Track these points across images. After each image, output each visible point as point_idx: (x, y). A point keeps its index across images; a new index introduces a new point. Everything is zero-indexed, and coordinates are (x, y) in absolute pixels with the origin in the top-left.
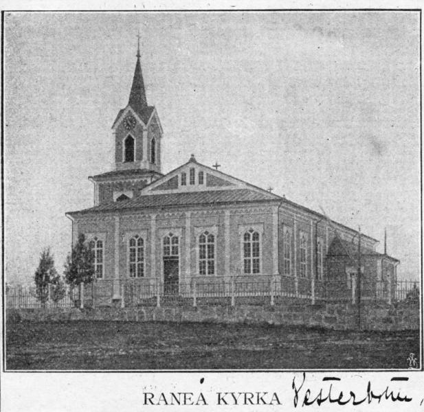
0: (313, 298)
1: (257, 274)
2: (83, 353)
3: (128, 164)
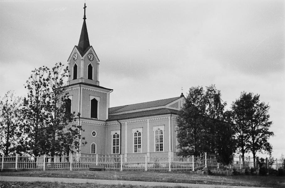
1: (161, 151)
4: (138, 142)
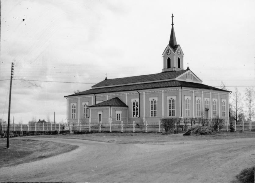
0: (146, 130)
3: (169, 69)
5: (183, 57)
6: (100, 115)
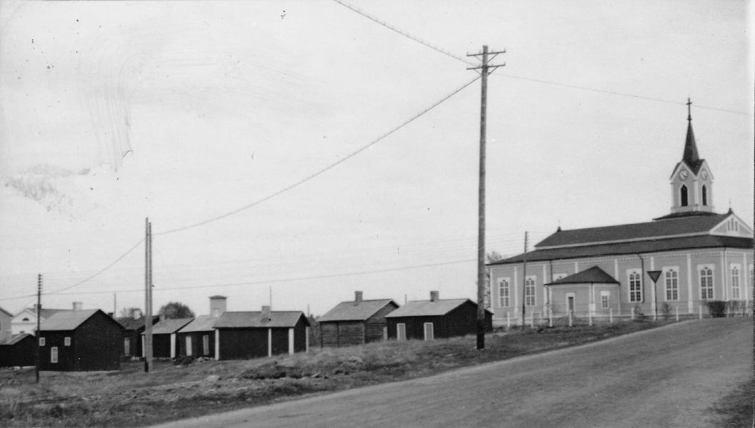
1: (675, 300)
2: (158, 397)
3: (686, 207)
4: (504, 292)
5: (711, 183)
6: (571, 298)
